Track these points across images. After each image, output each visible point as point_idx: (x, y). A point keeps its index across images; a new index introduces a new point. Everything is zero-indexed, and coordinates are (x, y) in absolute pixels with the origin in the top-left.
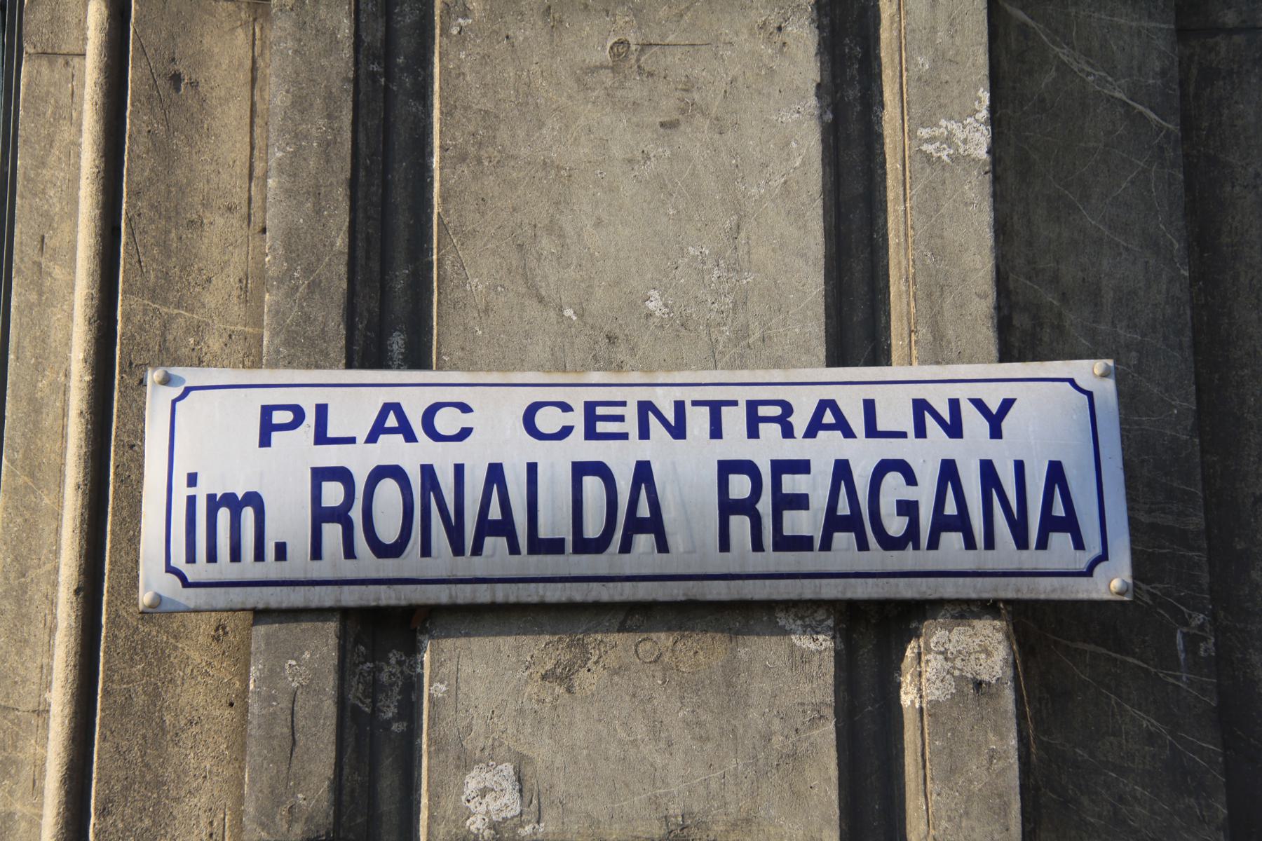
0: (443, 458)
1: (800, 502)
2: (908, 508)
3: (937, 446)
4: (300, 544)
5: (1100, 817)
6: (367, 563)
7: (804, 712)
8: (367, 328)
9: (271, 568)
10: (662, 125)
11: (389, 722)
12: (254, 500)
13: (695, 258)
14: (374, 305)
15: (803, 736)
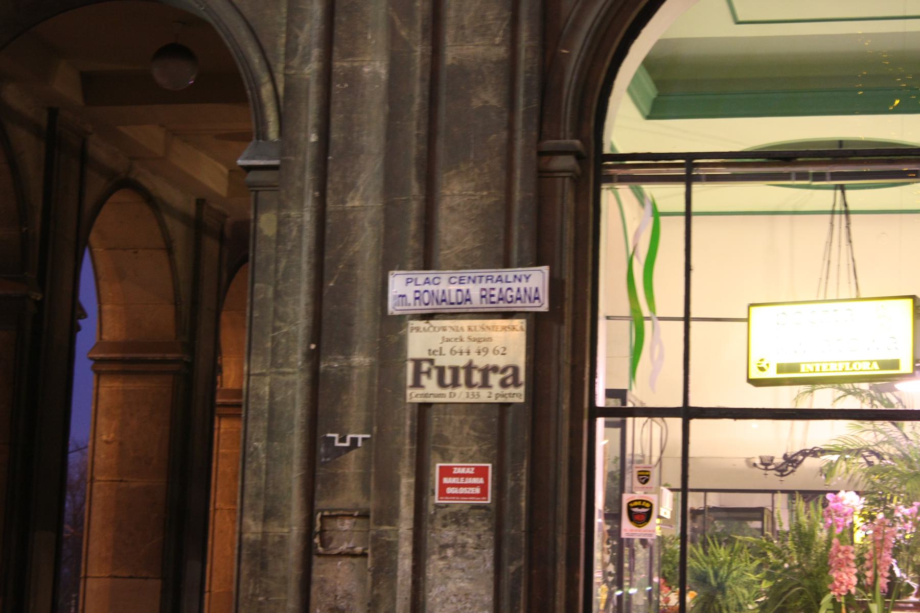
4: (412, 303)
6: (423, 307)
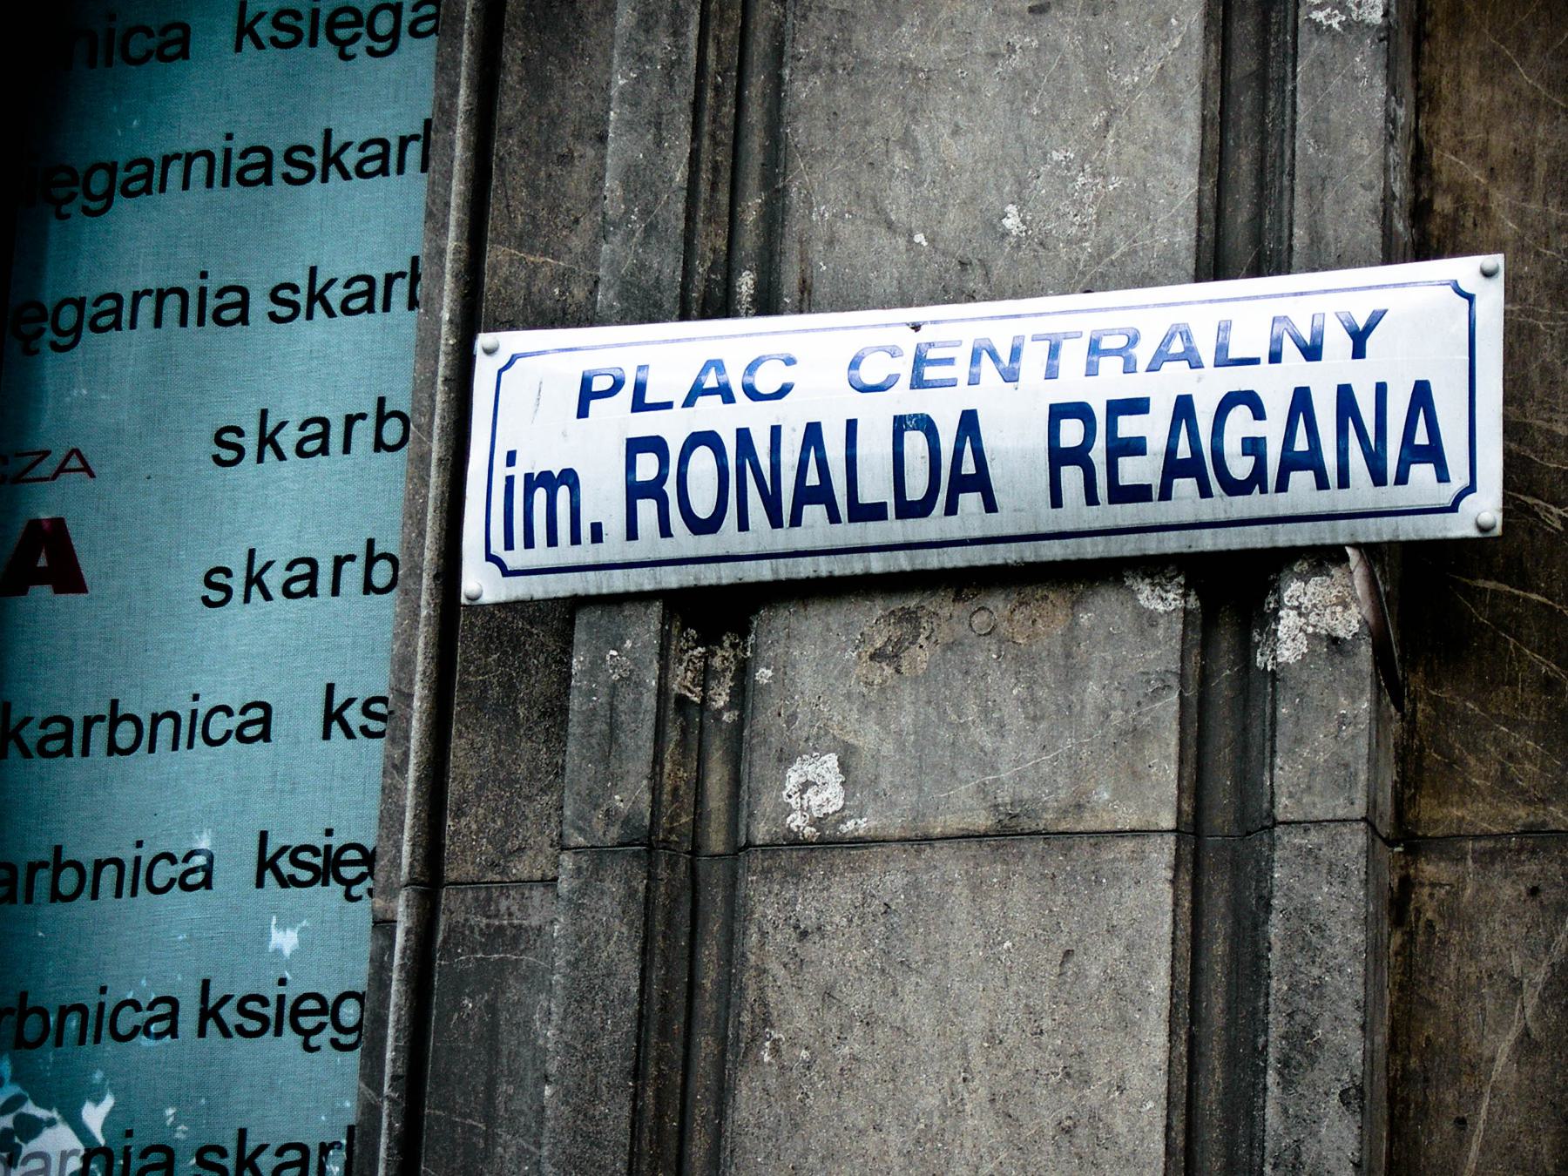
0: (758, 419)
1: (1136, 447)
2: (1253, 447)
3: (1294, 369)
4: (615, 526)
5: (1486, 777)
6: (684, 542)
7: (1148, 682)
8: (711, 270)
9: (586, 552)
10: (1031, 10)
11: (720, 712)
12: (569, 478)
13: (1058, 164)
14: (721, 244)
15: (1145, 709)
